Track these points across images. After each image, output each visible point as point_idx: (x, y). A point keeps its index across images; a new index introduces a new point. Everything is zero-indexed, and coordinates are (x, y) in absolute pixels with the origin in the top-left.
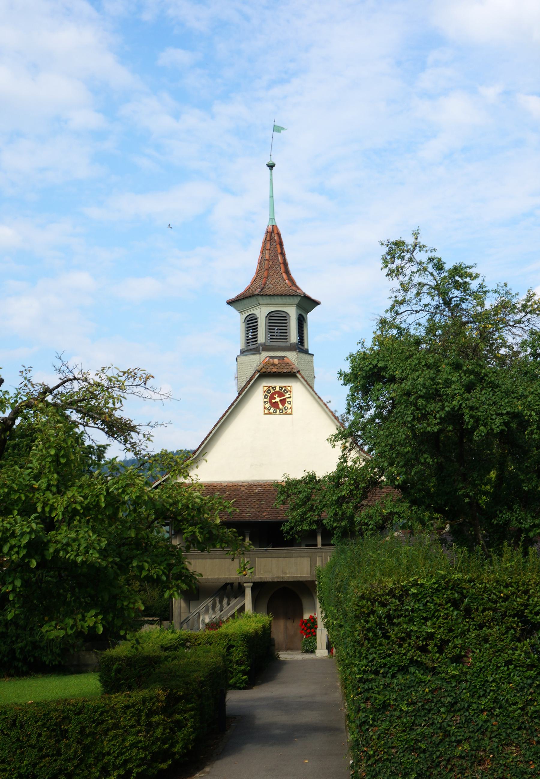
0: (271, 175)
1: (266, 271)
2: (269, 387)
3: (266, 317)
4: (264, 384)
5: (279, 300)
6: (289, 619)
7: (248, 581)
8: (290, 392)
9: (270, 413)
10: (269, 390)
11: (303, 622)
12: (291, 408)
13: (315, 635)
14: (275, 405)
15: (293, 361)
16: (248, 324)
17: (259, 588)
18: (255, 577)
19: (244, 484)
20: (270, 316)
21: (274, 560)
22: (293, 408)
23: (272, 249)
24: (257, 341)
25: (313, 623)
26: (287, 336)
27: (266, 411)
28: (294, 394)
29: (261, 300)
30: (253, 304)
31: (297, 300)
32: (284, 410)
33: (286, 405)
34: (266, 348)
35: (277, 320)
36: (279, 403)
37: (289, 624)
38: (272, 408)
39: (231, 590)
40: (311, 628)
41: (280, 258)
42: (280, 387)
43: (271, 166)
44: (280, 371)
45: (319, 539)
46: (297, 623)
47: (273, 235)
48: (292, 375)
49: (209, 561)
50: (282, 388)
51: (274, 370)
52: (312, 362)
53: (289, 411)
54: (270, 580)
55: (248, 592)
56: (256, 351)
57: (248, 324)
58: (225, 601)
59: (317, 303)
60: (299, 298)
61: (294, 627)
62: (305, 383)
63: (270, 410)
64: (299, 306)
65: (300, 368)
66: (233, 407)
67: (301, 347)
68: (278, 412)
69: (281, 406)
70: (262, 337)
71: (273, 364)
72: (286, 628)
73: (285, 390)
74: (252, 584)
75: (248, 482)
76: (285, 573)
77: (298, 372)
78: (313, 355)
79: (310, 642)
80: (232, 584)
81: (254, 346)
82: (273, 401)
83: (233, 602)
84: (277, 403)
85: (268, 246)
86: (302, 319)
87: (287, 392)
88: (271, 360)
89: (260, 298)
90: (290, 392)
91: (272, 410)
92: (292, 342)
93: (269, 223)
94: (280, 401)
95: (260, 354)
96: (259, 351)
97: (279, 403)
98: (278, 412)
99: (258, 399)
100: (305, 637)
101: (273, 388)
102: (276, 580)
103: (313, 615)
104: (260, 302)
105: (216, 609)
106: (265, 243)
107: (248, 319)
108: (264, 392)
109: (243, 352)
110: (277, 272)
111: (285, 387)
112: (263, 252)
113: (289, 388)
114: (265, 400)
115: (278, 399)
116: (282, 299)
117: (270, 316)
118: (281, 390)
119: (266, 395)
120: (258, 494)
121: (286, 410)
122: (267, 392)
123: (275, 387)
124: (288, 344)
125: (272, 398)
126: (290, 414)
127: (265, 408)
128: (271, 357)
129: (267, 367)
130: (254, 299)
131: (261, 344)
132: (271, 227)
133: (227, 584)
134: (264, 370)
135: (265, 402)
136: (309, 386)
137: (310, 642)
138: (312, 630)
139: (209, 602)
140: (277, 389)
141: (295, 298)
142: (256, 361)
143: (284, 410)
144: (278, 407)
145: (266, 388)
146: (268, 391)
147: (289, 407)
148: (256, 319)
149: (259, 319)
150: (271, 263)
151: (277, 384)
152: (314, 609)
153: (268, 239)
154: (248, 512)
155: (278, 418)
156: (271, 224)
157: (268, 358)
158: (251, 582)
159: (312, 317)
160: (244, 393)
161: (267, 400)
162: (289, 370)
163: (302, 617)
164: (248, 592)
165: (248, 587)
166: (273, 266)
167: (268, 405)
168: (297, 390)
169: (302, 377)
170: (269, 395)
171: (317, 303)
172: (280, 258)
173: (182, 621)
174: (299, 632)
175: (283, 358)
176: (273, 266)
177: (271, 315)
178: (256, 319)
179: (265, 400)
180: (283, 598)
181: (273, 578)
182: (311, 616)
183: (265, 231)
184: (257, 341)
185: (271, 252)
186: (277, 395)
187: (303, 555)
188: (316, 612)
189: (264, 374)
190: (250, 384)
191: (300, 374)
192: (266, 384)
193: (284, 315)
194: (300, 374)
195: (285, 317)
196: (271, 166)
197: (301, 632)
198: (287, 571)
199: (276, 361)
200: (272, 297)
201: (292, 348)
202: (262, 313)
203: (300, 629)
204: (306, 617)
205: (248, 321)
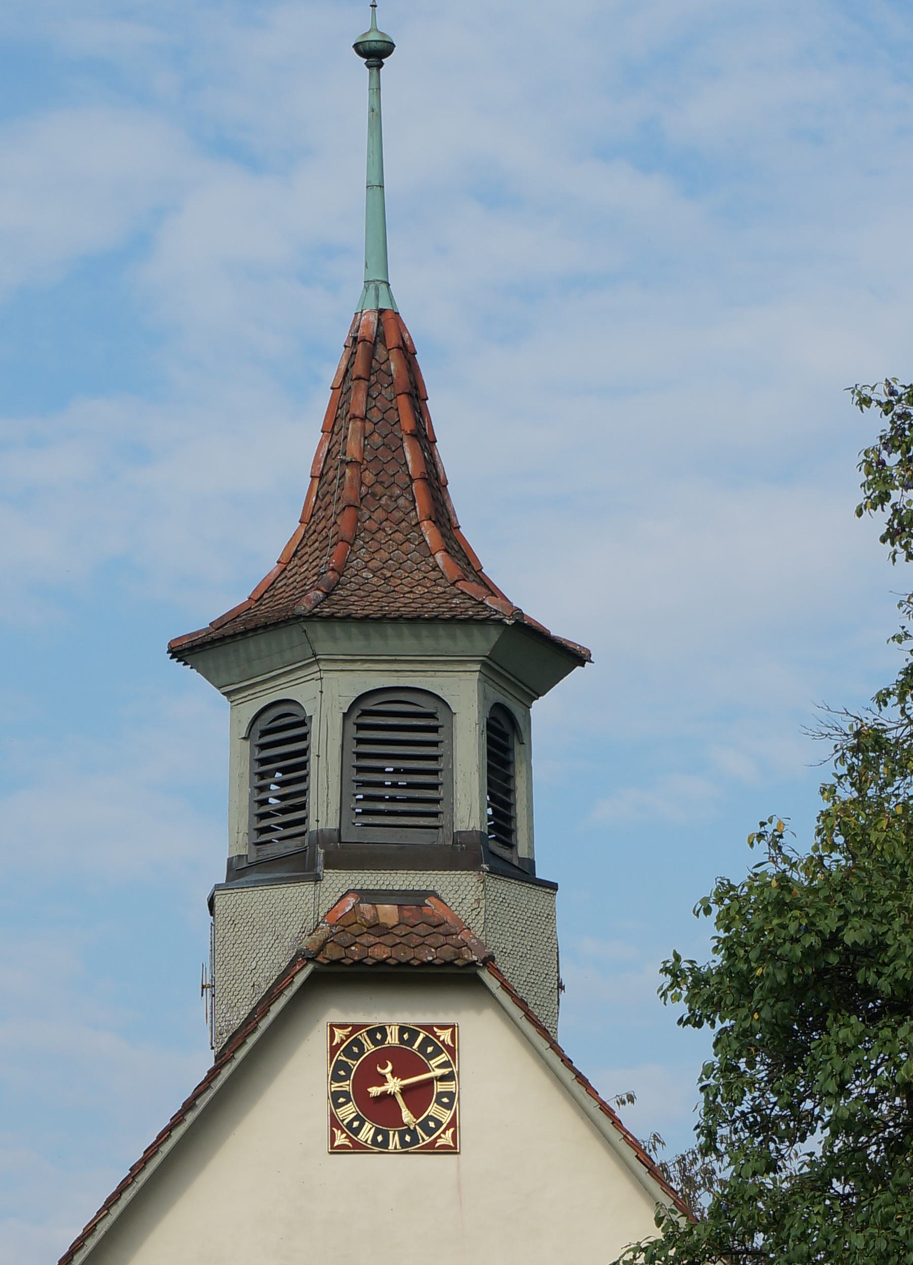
0: (376, 89)
1: (349, 513)
2: (357, 1028)
3: (345, 715)
4: (336, 1015)
5: (404, 641)
8: (452, 1051)
9: (357, 1148)
10: (357, 1043)
12: (453, 1123)
14: (381, 1110)
16: (263, 747)
20: (363, 712)
23: (375, 415)
24: (302, 821)
26: (436, 801)
27: (341, 1139)
29: (324, 640)
30: (288, 656)
31: (484, 642)
33: (433, 1109)
34: (344, 855)
35: (396, 732)
36: (399, 1099)
38: (367, 1126)
42: (402, 1030)
43: (375, 54)
44: (404, 955)
47: (381, 351)
50: (414, 1034)
51: (381, 953)
52: (550, 918)
56: (300, 867)
57: (263, 747)
59: (575, 657)
60: (494, 634)
63: (357, 1131)
64: (492, 669)
66: (190, 1117)
67: (499, 848)
68: (394, 1141)
69: (407, 1116)
71: (377, 928)
73: (426, 1042)
77: (488, 961)
81: (291, 846)
82: (375, 1091)
84: (393, 1103)
86: (507, 728)
87: (437, 1052)
88: (365, 907)
89: (319, 630)
92: (459, 827)
93: (364, 298)
94: (404, 1091)
95: (317, 879)
96: (314, 865)
97: (399, 1099)
98: (394, 1141)
99: (302, 1083)
101: (371, 1033)
104: (318, 648)
107: (262, 725)
108: (333, 1050)
109: (239, 872)
110: (398, 515)
111: (429, 1028)
113: (445, 1035)
114: (335, 1087)
115: (393, 1085)
116: (417, 637)
117: (366, 713)
118: (411, 1042)
119: (340, 1065)
121: (429, 1132)
122: (348, 1052)
123: (382, 1029)
124: (442, 838)
126: (450, 1150)
127: (335, 1122)
129: (346, 939)
130: (294, 634)
131: (321, 837)
132: (373, 318)
134: (333, 953)
136: (537, 1025)
140: (393, 1039)
141: (476, 631)
142: (297, 911)
144: (397, 1121)
145: (339, 1034)
146: (353, 1048)
148: (302, 723)
149: (314, 726)
150: (369, 477)
151: (393, 1014)
153: (359, 369)
155: (394, 1170)
156: (371, 305)
157: (351, 900)
159: (551, 716)
160: (242, 1058)
161: (347, 1086)
162: (447, 954)
166: (379, 489)
167: (348, 1112)
168: (483, 1046)
170: (355, 1064)
171: (575, 657)
175: (418, 897)
176: (379, 489)
177: (369, 705)
178: (302, 723)
179: (335, 1087)
184: (302, 821)
189: (333, 970)
191: (497, 973)
193: (428, 706)
194: (497, 973)
195: (431, 716)
196: (375, 54)
199: (388, 913)
201: (459, 855)
202: (326, 696)
205: (264, 733)
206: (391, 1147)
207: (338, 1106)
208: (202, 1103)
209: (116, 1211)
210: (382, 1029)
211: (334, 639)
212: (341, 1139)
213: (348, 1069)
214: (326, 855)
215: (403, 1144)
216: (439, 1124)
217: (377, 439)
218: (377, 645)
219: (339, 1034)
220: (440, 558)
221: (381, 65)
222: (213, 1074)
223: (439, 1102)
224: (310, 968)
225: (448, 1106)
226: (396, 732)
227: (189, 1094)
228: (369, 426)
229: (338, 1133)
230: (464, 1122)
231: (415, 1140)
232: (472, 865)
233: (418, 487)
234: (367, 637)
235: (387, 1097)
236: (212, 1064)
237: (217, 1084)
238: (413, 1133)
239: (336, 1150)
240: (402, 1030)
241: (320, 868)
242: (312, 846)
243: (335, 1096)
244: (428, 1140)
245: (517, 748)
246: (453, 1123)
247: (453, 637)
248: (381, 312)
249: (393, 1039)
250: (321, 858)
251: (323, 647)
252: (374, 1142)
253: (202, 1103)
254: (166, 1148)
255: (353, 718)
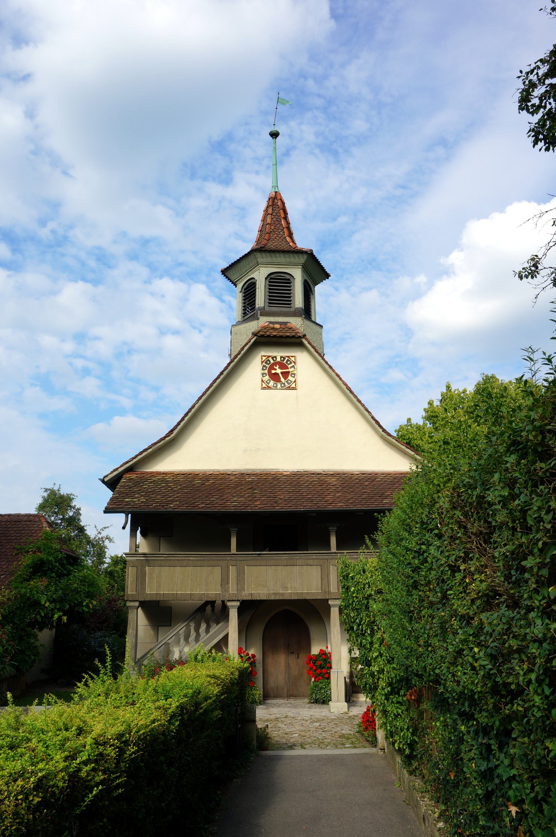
1: (268, 235)
2: (269, 357)
3: (266, 279)
4: (263, 353)
5: (281, 258)
6: (293, 653)
7: (234, 599)
8: (295, 363)
9: (269, 388)
10: (269, 360)
11: (311, 658)
12: (295, 381)
13: (329, 678)
14: (275, 377)
15: (298, 327)
17: (250, 609)
18: (243, 593)
19: (234, 473)
20: (271, 279)
21: (271, 570)
22: (298, 381)
23: (274, 214)
25: (325, 660)
26: (290, 287)
28: (299, 365)
30: (251, 265)
31: (302, 259)
32: (286, 384)
33: (290, 378)
35: (279, 286)
36: (280, 374)
37: (292, 660)
39: (210, 612)
40: (322, 667)
41: (283, 222)
42: (281, 357)
43: (274, 135)
44: (281, 334)
45: (333, 541)
46: (303, 659)
47: (276, 201)
48: (294, 341)
49: (178, 569)
50: (284, 358)
51: (275, 334)
52: (321, 334)
53: (293, 385)
54: (265, 598)
55: (233, 615)
56: (255, 318)
58: (203, 627)
60: (305, 257)
61: (298, 664)
62: (312, 350)
63: (269, 383)
64: (305, 269)
65: (305, 332)
66: (222, 377)
67: (307, 312)
68: (279, 386)
69: (282, 379)
70: (260, 300)
71: (273, 328)
72: (288, 666)
73: (288, 360)
74: (238, 604)
75: (240, 471)
76: (286, 588)
77: (304, 336)
78: (322, 326)
79: (321, 688)
80: (212, 603)
82: (273, 372)
83: (215, 628)
85: (270, 211)
90: (295, 363)
91: (272, 383)
92: (296, 306)
94: (282, 373)
95: (258, 319)
97: (280, 374)
98: (279, 386)
99: (254, 370)
100: (313, 679)
101: (273, 358)
102: (273, 598)
103: (324, 648)
105: (190, 640)
106: (266, 210)
108: (262, 362)
110: (280, 236)
111: (288, 357)
112: (264, 220)
113: (293, 359)
114: (263, 372)
115: (279, 371)
116: (285, 257)
117: (271, 278)
118: (283, 360)
119: (264, 366)
120: (251, 482)
121: (289, 384)
122: (266, 363)
123: (276, 357)
124: (292, 309)
125: (272, 368)
128: (271, 323)
129: (265, 331)
131: (260, 309)
132: (274, 193)
133: (207, 603)
134: (261, 333)
135: (263, 374)
136: (318, 355)
137: (321, 688)
138: (323, 671)
139: (180, 628)
140: (279, 359)
141: (300, 256)
143: (286, 384)
144: (279, 381)
145: (264, 358)
147: (293, 380)
150: (273, 227)
151: (279, 354)
152: (325, 638)
153: (270, 204)
154: (235, 501)
155: (278, 395)
157: (267, 323)
158: (238, 600)
159: (319, 289)
161: (266, 371)
162: (293, 334)
163: (310, 651)
164: (233, 615)
165: (233, 607)
166: (275, 230)
167: (267, 378)
168: (303, 362)
169: (309, 343)
170: (268, 366)
172: (283, 222)
173: (139, 656)
174: (305, 671)
175: (286, 323)
176: (275, 230)
177: (272, 276)
179: (263, 372)
180: (285, 624)
181: (269, 594)
182: (321, 650)
183: (278, 468)
185: (273, 217)
186: (278, 366)
187: (311, 562)
188: (513, 832)
189: (263, 340)
190: (245, 350)
191: (307, 339)
192: (263, 353)
195: (289, 280)
196: (274, 135)
197: (309, 672)
198: (289, 585)
199: (277, 326)
200: (273, 255)
201: (296, 313)
202: (260, 275)
203: (307, 667)
204: (315, 650)
206: (278, 388)
207: (263, 377)
208: (225, 373)
209: (201, 402)
210: (276, 357)
211: (263, 258)
212: (264, 385)
213: (266, 367)
214: (261, 313)
215: (282, 387)
216: (291, 381)
217: (275, 219)
218: (274, 260)
219: (264, 358)
220: (291, 244)
221: (276, 138)
222: (229, 364)
223: (291, 376)
224: (255, 337)
225: (294, 377)
226: (279, 286)
227: (222, 369)
228: (273, 217)
229: (263, 384)
230: (298, 381)
231: (285, 386)
232: (300, 316)
233: (285, 230)
234: (271, 257)
235: (276, 374)
236: (229, 362)
237: (230, 368)
238: (284, 384)
239: (263, 388)
240: (281, 357)
241: (259, 316)
242: (257, 312)
243: (263, 374)
244: (288, 386)
245: (312, 296)
246: (295, 381)
247: (295, 258)
248: (276, 192)
249: (279, 359)
250: (259, 314)
251: (260, 260)
252: (273, 386)
253: (225, 373)
254: (215, 385)
255: (268, 279)
